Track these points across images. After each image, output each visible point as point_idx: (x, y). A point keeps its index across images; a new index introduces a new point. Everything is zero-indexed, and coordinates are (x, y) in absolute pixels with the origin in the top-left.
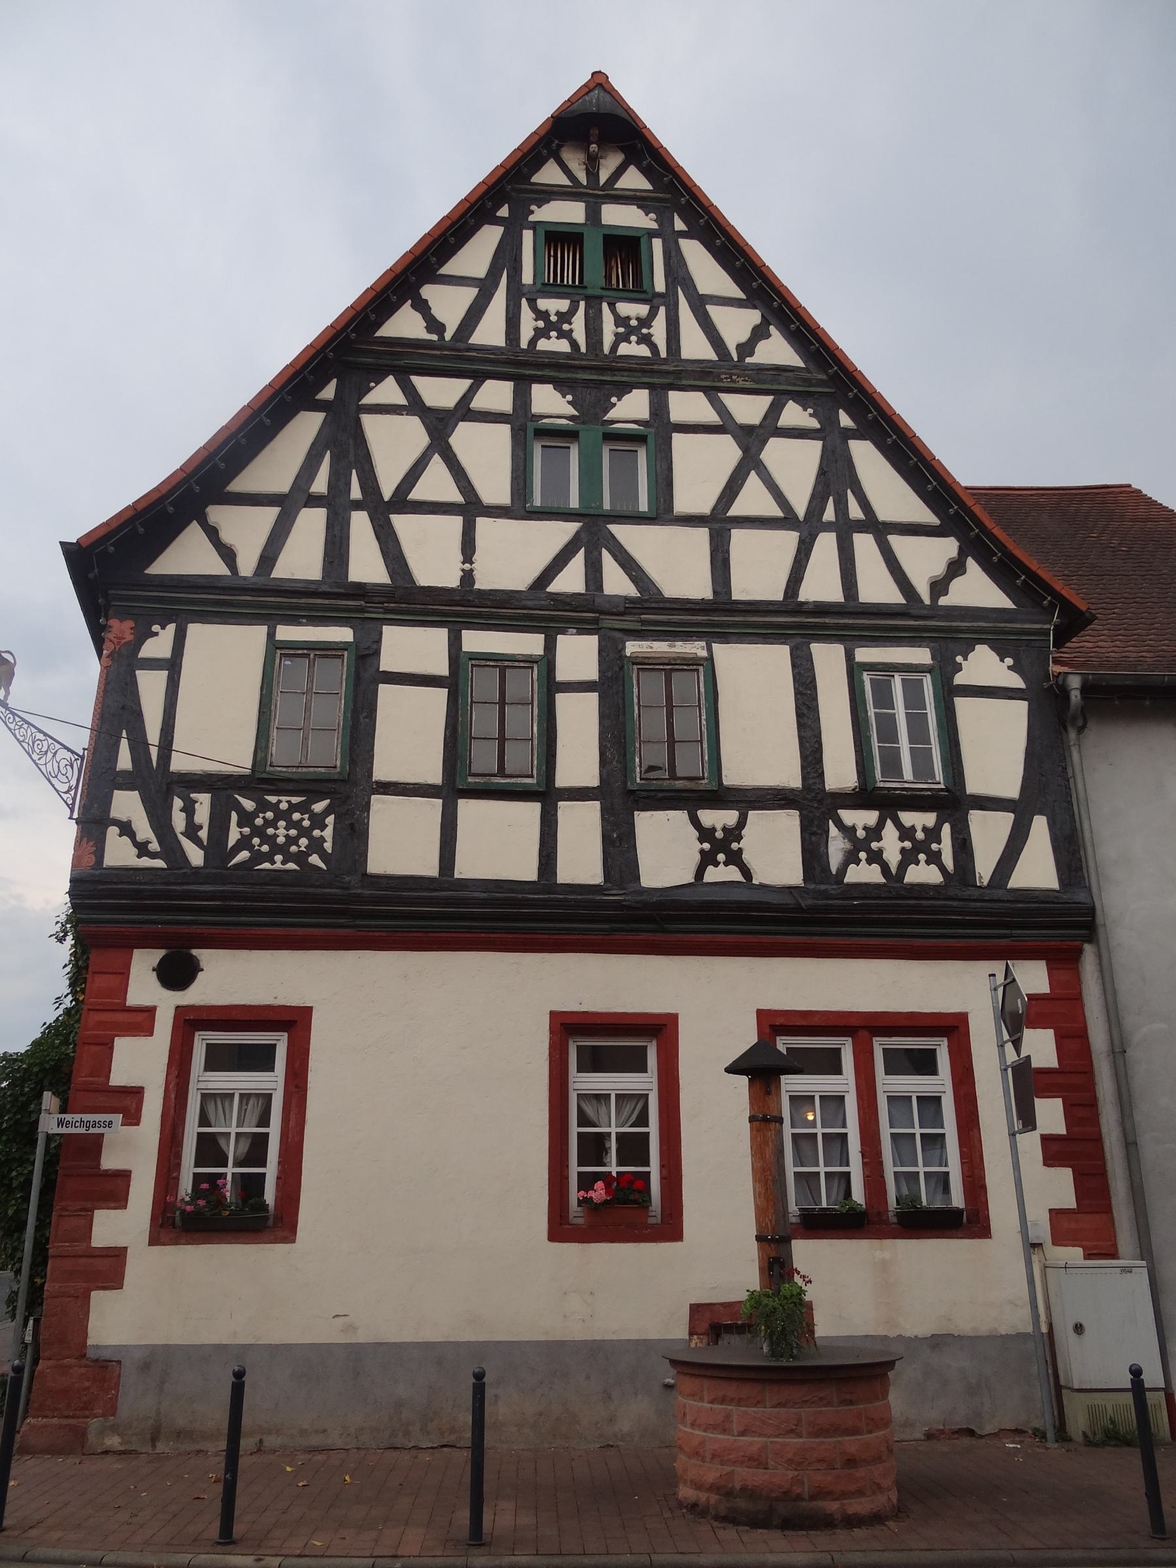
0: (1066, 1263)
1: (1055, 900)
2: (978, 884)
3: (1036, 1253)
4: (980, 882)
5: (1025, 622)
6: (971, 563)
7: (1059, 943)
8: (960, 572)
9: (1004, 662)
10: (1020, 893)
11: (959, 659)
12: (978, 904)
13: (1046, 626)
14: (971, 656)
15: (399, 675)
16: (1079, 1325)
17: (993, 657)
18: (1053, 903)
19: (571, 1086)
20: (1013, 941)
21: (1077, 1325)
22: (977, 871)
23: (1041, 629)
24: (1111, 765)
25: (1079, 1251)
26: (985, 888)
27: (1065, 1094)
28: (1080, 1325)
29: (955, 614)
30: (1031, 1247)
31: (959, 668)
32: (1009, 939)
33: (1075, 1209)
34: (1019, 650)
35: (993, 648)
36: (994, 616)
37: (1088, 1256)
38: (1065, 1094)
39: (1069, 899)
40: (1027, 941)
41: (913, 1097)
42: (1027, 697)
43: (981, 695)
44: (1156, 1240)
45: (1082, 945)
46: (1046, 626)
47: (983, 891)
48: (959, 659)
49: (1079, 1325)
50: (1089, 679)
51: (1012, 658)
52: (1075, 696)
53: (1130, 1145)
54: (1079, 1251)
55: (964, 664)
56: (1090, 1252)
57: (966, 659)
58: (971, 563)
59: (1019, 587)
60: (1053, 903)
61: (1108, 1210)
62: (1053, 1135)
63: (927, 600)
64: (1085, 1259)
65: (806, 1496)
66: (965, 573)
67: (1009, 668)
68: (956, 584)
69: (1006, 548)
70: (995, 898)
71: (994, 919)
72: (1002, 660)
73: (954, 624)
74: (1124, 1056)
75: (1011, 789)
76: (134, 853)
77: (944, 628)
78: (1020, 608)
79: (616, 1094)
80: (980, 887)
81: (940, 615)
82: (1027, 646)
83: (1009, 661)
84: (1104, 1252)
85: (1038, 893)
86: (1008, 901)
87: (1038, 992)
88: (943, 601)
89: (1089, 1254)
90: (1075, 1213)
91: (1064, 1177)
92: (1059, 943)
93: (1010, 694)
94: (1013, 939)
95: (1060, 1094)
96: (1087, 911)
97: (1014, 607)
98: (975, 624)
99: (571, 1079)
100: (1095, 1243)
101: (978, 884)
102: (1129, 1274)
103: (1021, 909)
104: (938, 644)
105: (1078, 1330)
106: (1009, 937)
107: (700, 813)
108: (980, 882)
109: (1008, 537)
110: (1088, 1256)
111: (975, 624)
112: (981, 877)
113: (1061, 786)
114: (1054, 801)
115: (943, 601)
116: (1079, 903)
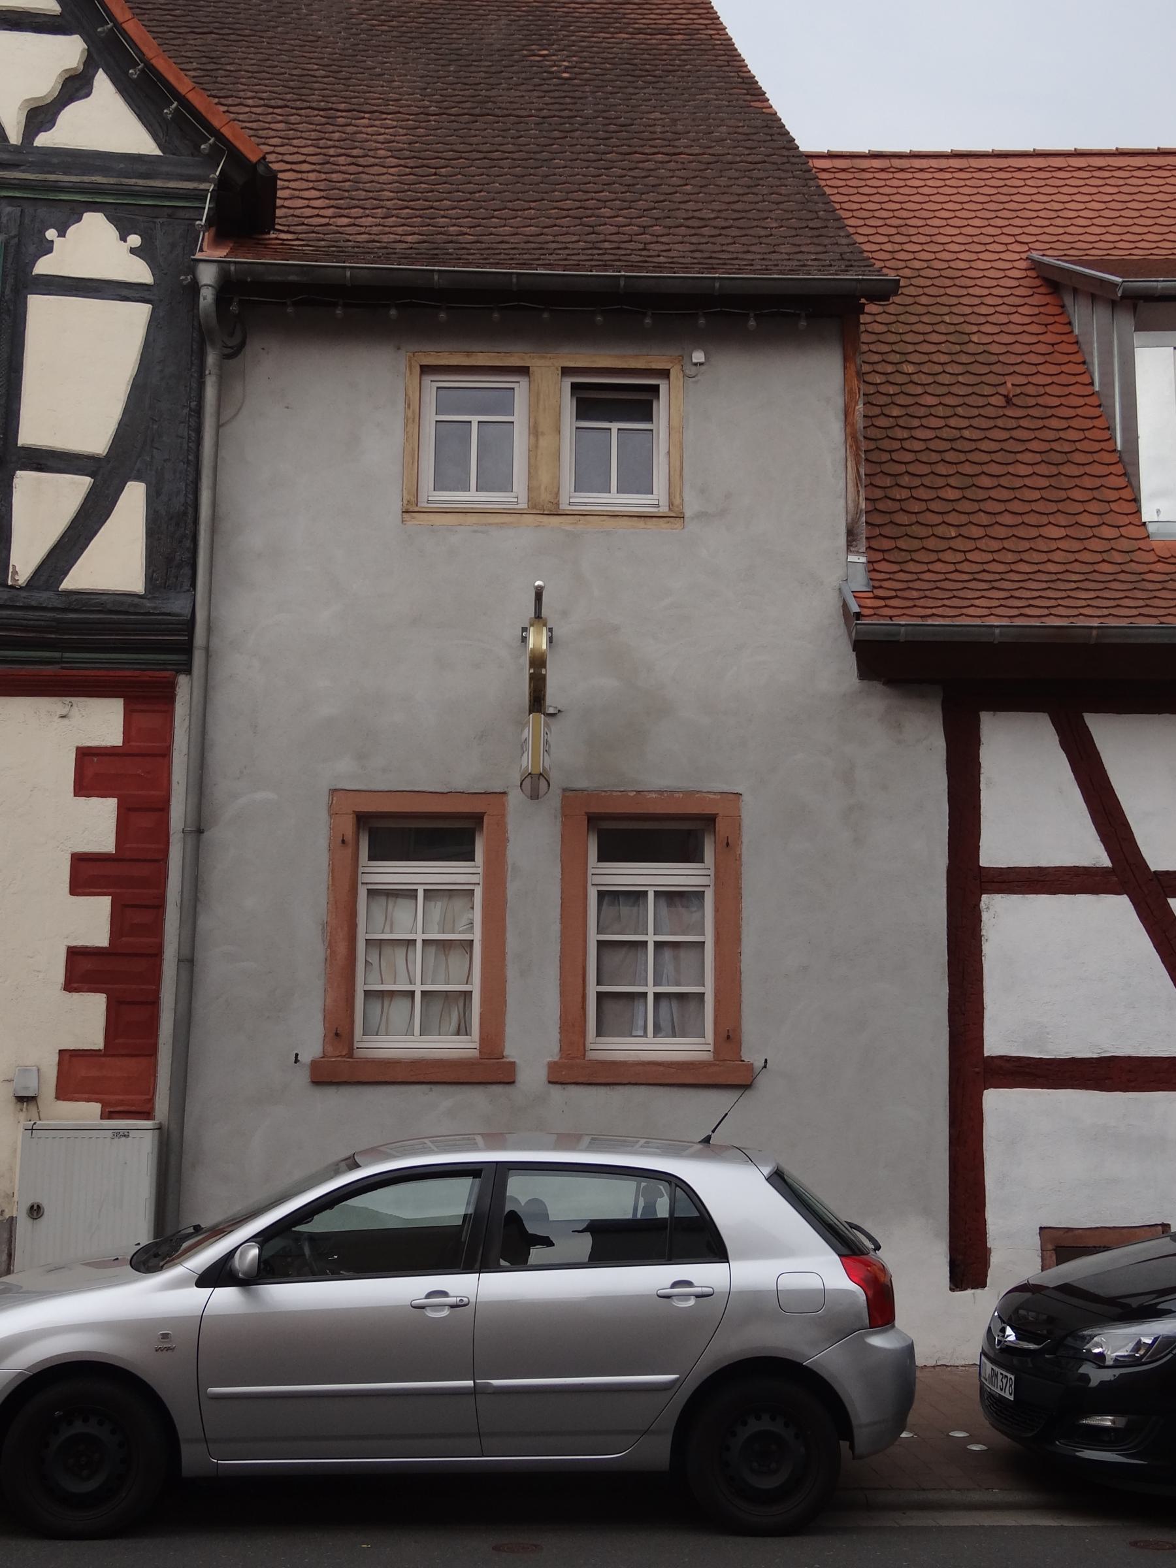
0: (35, 1123)
1: (132, 610)
2: (10, 583)
3: (24, 1110)
4: (13, 579)
5: (169, 176)
6: (102, 82)
7: (137, 673)
8: (83, 92)
9: (125, 241)
10: (75, 597)
11: (51, 234)
12: (160, 617)
13: (203, 186)
14: (72, 230)
15: (61, 279)
16: (35, 1207)
17: (111, 232)
18: (126, 613)
19: (592, 879)
20: (63, 668)
21: (32, 1207)
22: (12, 563)
23: (195, 189)
24: (288, 408)
25: (96, 1107)
26: (21, 588)
27: (118, 891)
28: (38, 1207)
29: (55, 161)
30: (19, 1101)
31: (48, 248)
32: (58, 666)
33: (100, 1050)
34: (155, 223)
35: (111, 219)
36: (122, 166)
37: (107, 1115)
38: (118, 891)
39: (155, 608)
40: (78, 669)
41: (649, 892)
42: (152, 297)
43: (74, 292)
44: (744, 1083)
45: (175, 677)
46: (203, 186)
47: (14, 592)
48: (51, 234)
49: (35, 1207)
50: (230, 270)
51: (140, 236)
52: (207, 296)
53: (188, 962)
54: (96, 1107)
55: (58, 243)
56: (112, 1110)
57: (62, 234)
58: (102, 82)
59: (165, 119)
60: (126, 613)
61: (151, 1052)
62: (87, 947)
63: (14, 136)
64: (102, 1118)
65: (1109, 1362)
66: (88, 95)
67: (133, 251)
68: (70, 115)
69: (144, 55)
70: (34, 603)
71: (31, 635)
72: (123, 238)
73: (52, 177)
74: (198, 841)
75: (96, 441)
76: (832, 578)
77: (33, 183)
78: (167, 155)
79: (424, 890)
80: (12, 587)
81: (29, 162)
82: (170, 216)
83: (135, 240)
84: (133, 1109)
85: (104, 598)
86: (54, 609)
87: (104, 744)
88: (43, 140)
89: (110, 1112)
90: (101, 1056)
91: (94, 1006)
92: (137, 673)
93: (125, 292)
94: (64, 665)
95: (110, 890)
96: (180, 626)
97: (158, 152)
98: (86, 179)
99: (591, 871)
100: (121, 1097)
101: (10, 583)
102: (123, 1139)
103: (73, 621)
104: (19, 209)
105: (33, 1215)
106: (58, 663)
107: (86, 482)
108: (13, 579)
109: (150, 36)
110: (107, 1115)
111: (86, 179)
112: (15, 572)
113: (182, 437)
114: (165, 461)
115: (43, 140)
116: (169, 614)
